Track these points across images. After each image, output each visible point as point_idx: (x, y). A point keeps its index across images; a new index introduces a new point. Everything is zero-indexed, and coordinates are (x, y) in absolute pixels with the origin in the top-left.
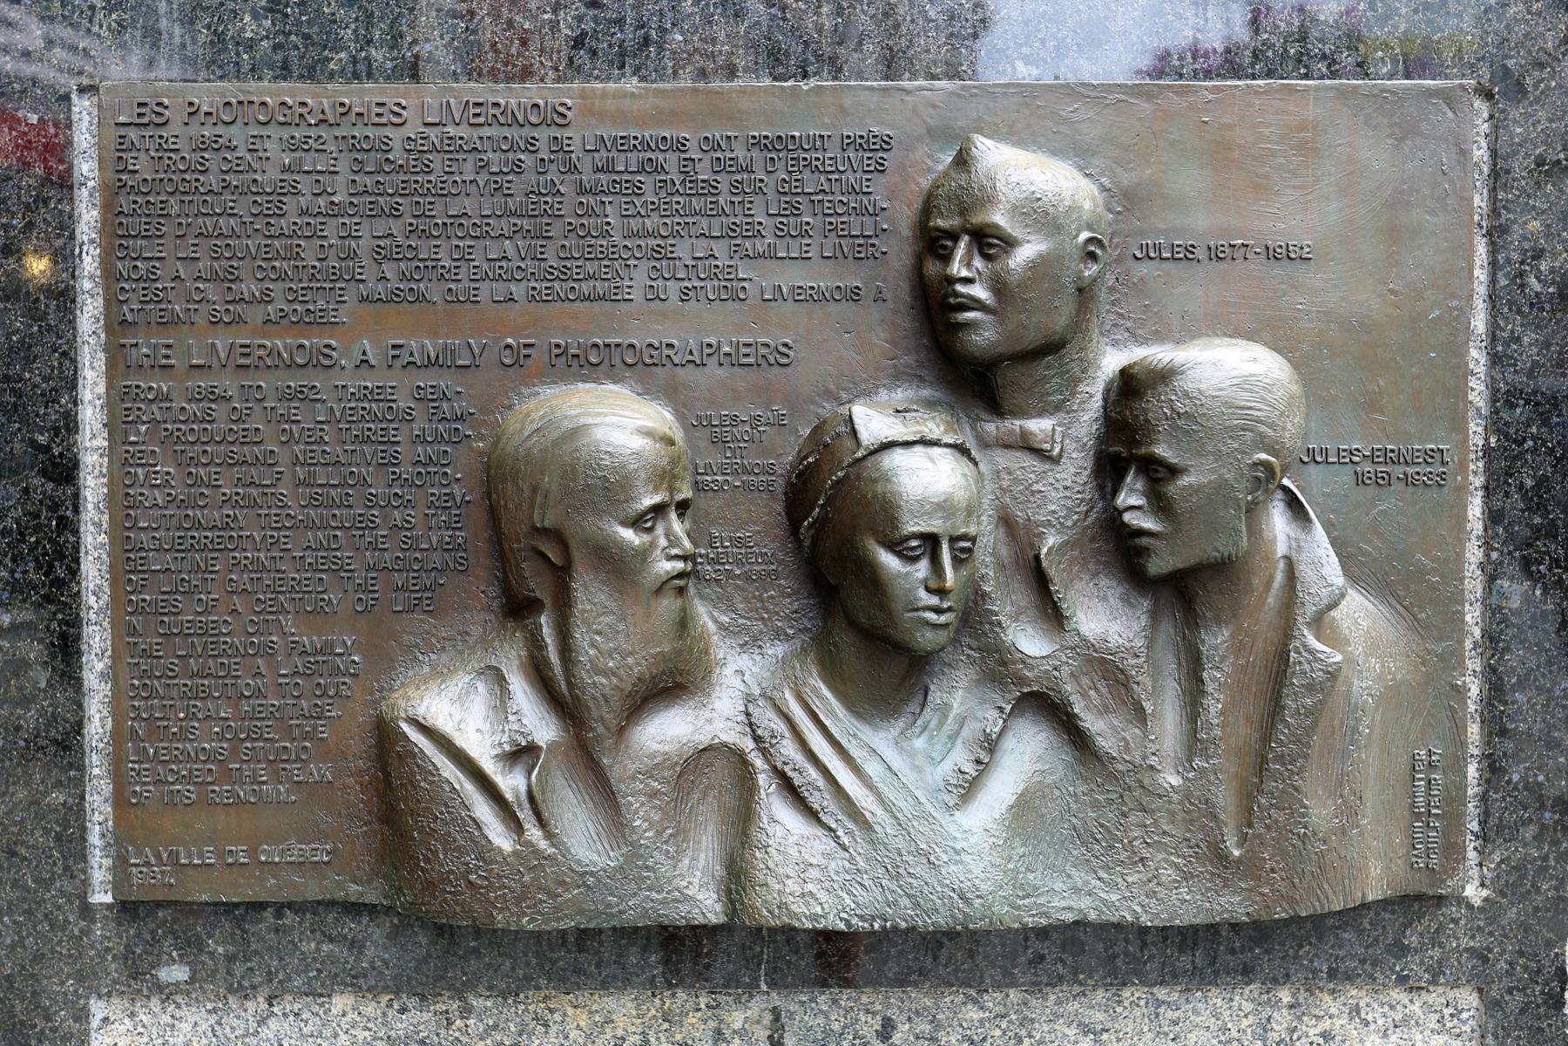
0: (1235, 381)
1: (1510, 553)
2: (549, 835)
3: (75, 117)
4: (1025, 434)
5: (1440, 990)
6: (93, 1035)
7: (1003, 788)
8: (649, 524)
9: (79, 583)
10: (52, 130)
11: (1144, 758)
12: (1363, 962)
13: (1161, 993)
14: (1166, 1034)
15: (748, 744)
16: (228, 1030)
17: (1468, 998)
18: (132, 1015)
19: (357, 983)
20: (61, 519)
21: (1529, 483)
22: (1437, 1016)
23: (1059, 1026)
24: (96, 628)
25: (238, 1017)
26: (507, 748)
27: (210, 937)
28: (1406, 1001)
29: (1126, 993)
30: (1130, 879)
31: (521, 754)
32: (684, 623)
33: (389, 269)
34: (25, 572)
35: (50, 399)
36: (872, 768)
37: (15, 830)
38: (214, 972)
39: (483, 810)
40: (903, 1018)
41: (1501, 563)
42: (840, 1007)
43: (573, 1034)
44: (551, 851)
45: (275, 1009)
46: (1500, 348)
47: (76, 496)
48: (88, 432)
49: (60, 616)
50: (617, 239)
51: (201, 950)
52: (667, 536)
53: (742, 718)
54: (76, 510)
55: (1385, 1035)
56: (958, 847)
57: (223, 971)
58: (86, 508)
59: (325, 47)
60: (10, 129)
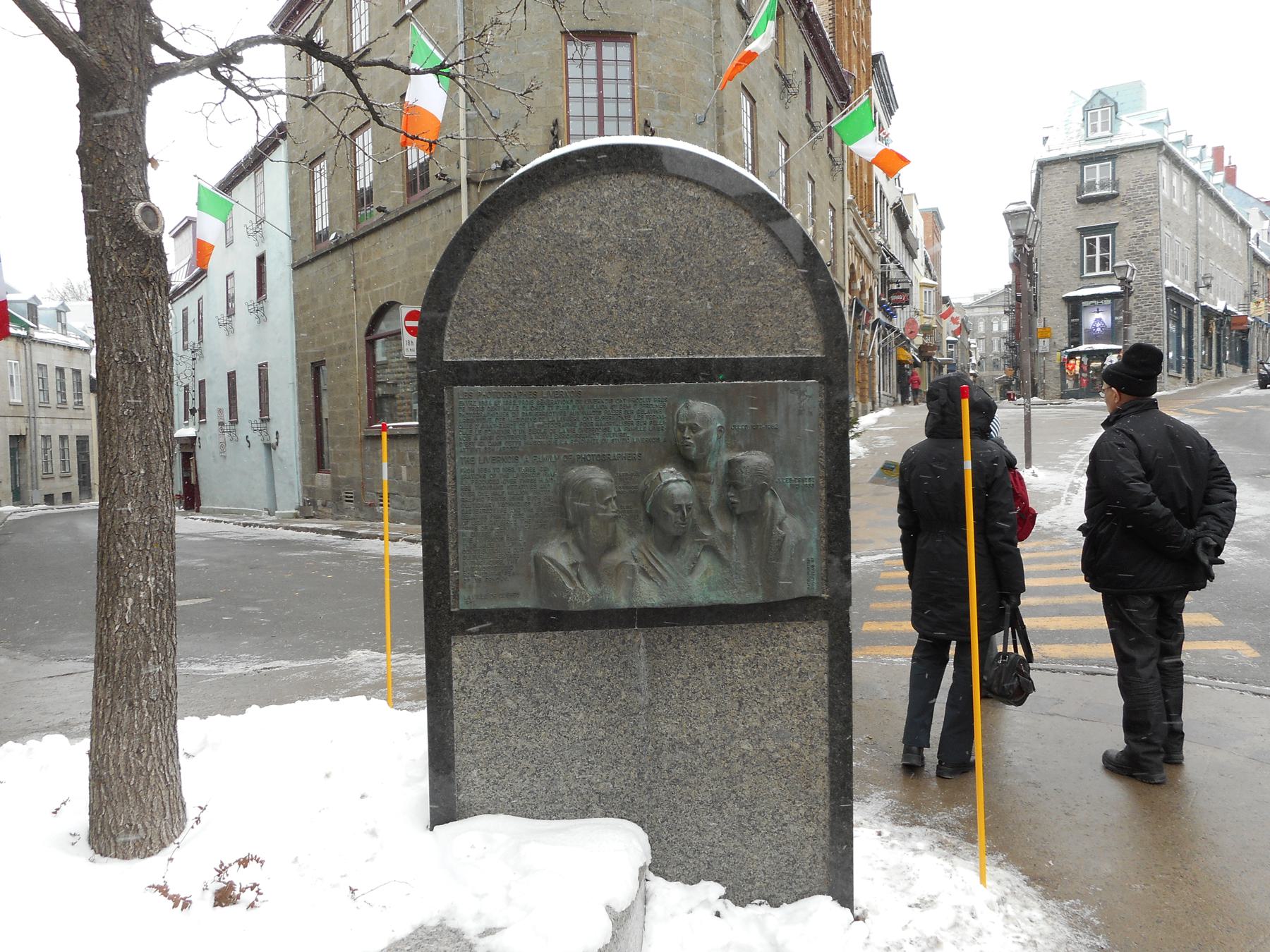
7: (700, 571)
17: (825, 624)
31: (574, 565)
39: (564, 578)
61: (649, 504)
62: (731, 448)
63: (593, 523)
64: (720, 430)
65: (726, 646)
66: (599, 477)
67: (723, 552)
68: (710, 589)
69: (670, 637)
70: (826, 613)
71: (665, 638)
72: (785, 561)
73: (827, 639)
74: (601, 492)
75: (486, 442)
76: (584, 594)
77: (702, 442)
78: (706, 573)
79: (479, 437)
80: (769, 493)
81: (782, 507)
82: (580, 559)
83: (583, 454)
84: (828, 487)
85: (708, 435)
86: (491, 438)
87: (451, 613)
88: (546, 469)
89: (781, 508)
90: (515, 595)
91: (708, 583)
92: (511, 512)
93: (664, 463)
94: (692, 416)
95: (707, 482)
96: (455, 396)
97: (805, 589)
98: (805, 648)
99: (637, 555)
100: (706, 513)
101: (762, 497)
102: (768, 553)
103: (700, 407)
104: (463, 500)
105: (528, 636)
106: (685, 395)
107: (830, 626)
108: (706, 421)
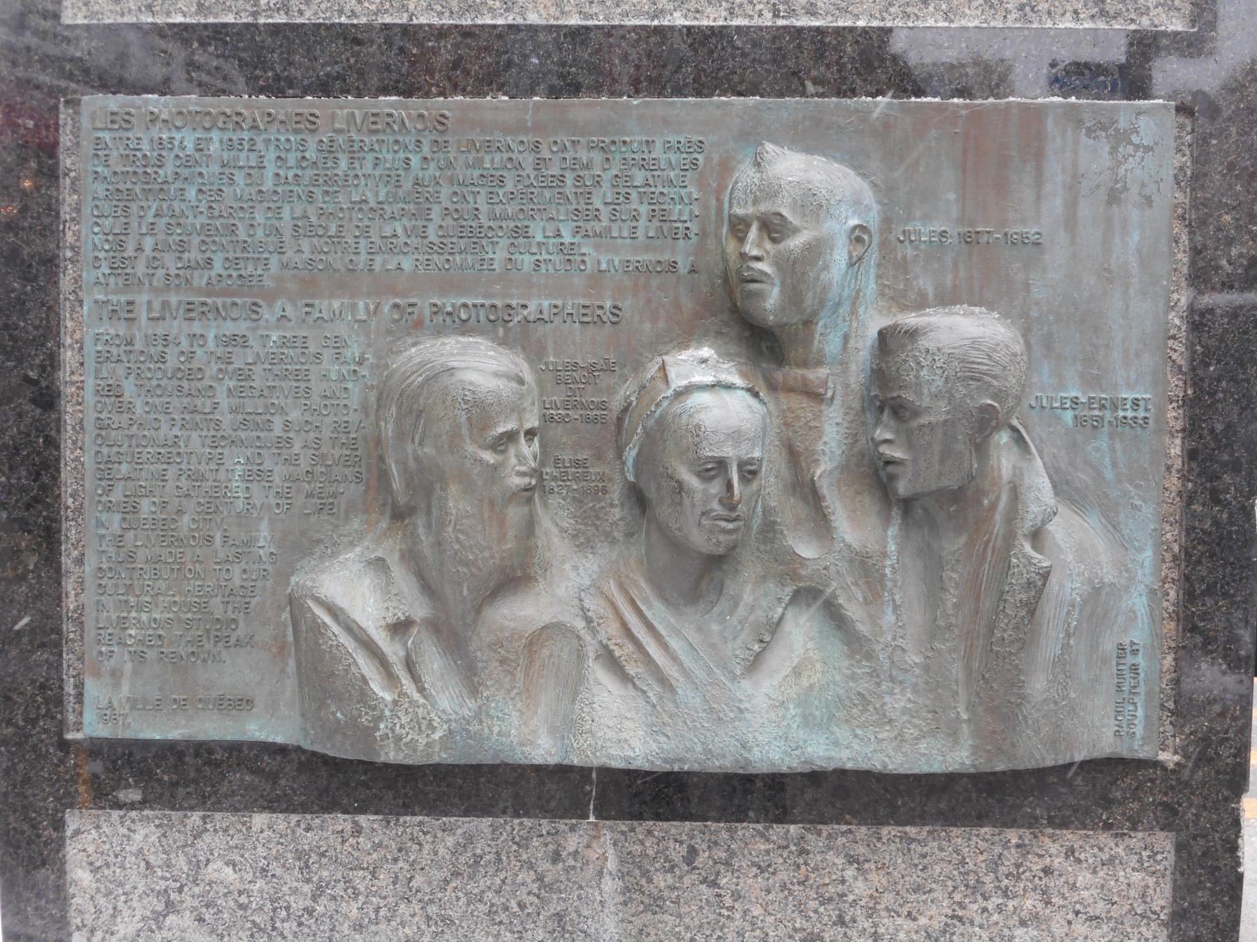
0: (966, 342)
1: (1202, 484)
2: (421, 690)
3: (61, 122)
4: (805, 381)
5: (1140, 835)
6: (68, 841)
7: (781, 660)
8: (502, 448)
9: (59, 488)
10: (44, 133)
11: (894, 639)
12: (1076, 811)
13: (911, 830)
14: (916, 866)
15: (580, 624)
16: (171, 842)
17: (1164, 842)
18: (98, 827)
19: (272, 804)
20: (47, 437)
21: (1219, 427)
22: (1137, 857)
23: (830, 856)
24: (72, 523)
25: (179, 832)
26: (389, 621)
27: (158, 766)
28: (1113, 845)
29: (885, 831)
30: (880, 736)
31: (399, 628)
32: (530, 526)
33: (305, 245)
34: (19, 479)
35: (40, 342)
36: (674, 643)
37: (9, 680)
38: (162, 795)
39: (365, 666)
40: (704, 846)
41: (1195, 492)
42: (654, 836)
43: (442, 851)
44: (422, 701)
45: (208, 826)
46: (1197, 318)
47: (59, 419)
48: (68, 369)
49: (45, 513)
50: (483, 219)
51: (151, 778)
52: (517, 456)
53: (577, 602)
54: (58, 431)
55: (1095, 872)
56: (742, 707)
57: (167, 794)
58: (66, 430)
59: (255, 68)
60: (13, 132)
61: (631, 454)
62: (900, 301)
63: (456, 502)
64: (858, 236)
65: (860, 888)
66: (481, 367)
67: (853, 610)
68: (808, 722)
69: (693, 852)
70: (1170, 809)
71: (677, 852)
72: (1050, 644)
73: (1167, 888)
74: (480, 413)
75: (169, 260)
76: (425, 715)
77: (794, 272)
78: (797, 672)
79: (148, 243)
80: (1004, 437)
81: (1044, 483)
82: (420, 610)
83: (449, 302)
84: (1191, 430)
85: (816, 250)
86: (182, 247)
87: (64, 745)
88: (339, 344)
89: (1040, 489)
90: (244, 704)
91: (803, 702)
92: (236, 461)
93: (686, 335)
94: (770, 191)
95: (814, 395)
96: (85, 122)
97: (1109, 733)
98: (1100, 908)
99: (594, 605)
100: (806, 491)
101: (981, 448)
102: (997, 623)
103: (791, 167)
104: (102, 426)
105: (281, 821)
106: (751, 135)
107: (1180, 848)
108: (812, 205)
